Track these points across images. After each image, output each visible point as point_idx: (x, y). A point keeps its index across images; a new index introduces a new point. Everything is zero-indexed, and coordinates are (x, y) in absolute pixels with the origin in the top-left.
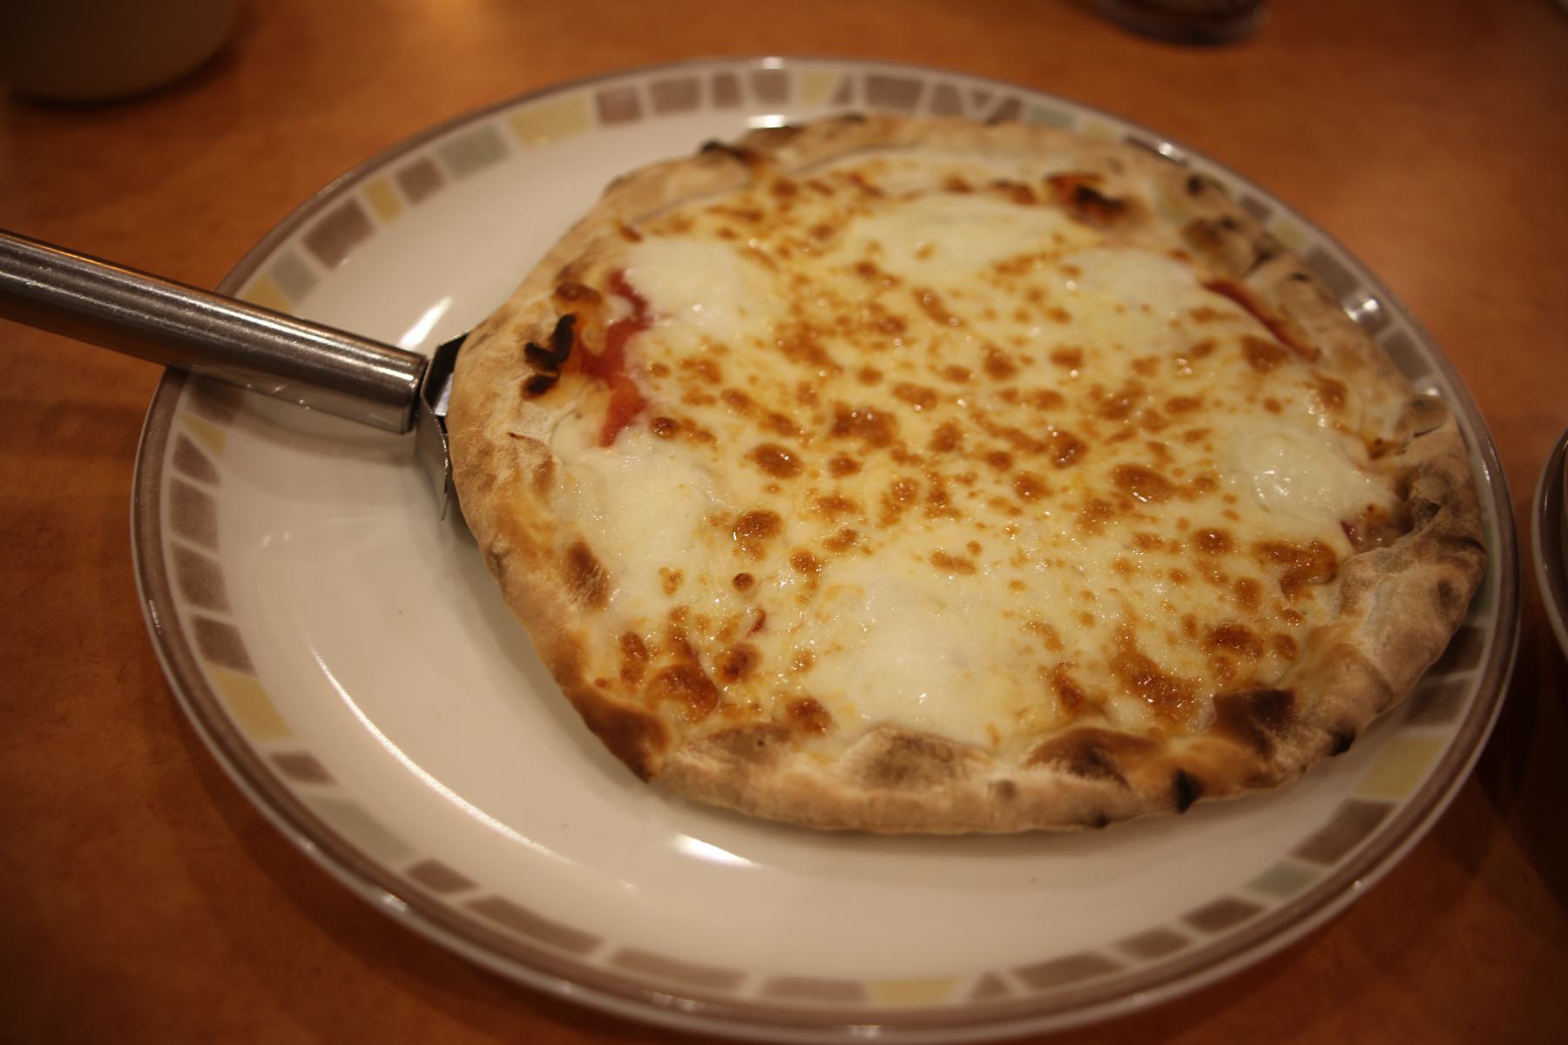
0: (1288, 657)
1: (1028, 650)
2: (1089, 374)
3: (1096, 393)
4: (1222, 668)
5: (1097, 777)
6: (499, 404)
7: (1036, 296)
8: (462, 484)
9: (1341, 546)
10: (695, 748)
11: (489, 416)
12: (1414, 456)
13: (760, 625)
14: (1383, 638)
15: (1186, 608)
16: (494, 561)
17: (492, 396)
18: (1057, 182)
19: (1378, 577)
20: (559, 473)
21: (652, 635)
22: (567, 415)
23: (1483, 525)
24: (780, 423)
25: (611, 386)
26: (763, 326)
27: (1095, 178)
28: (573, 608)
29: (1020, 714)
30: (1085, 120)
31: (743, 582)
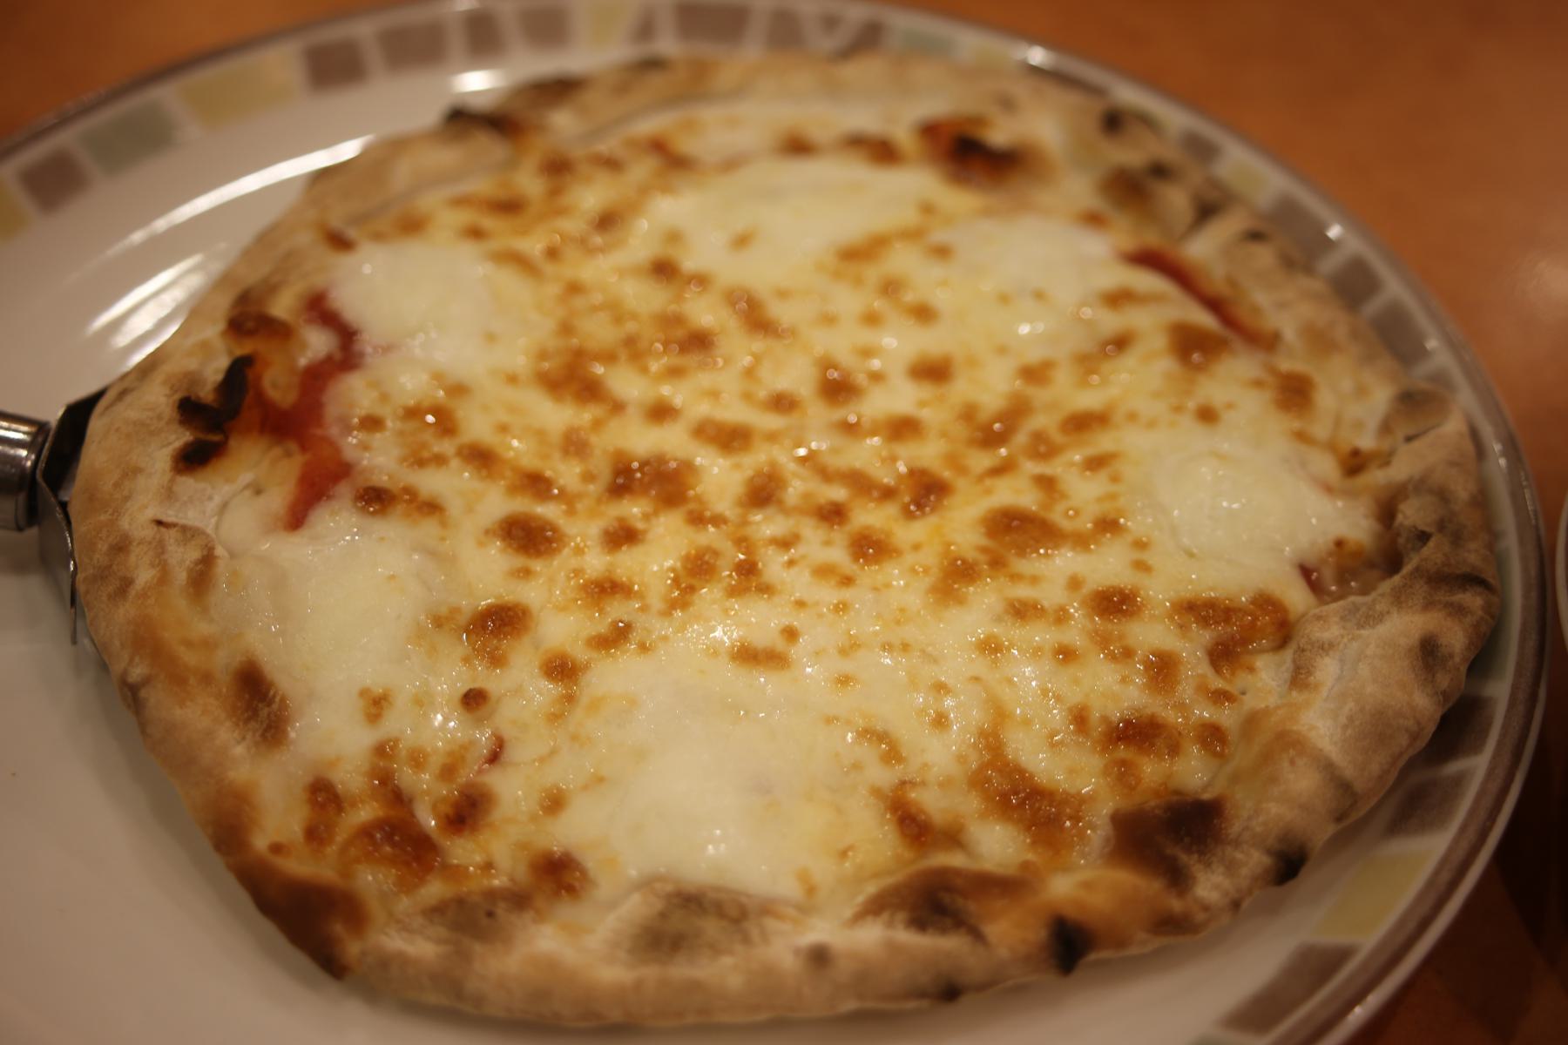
0: (1215, 754)
1: (857, 766)
2: (961, 389)
3: (968, 413)
4: (1123, 774)
5: (943, 931)
6: (141, 481)
7: (890, 288)
8: (87, 592)
9: (1296, 597)
10: (405, 928)
11: (127, 498)
12: (1401, 469)
13: (495, 757)
14: (1343, 720)
15: (1075, 696)
16: (129, 694)
17: (132, 472)
18: (930, 131)
19: (1342, 636)
20: (222, 568)
21: (351, 776)
22: (242, 491)
23: (1500, 562)
24: (536, 484)
25: (304, 448)
26: (519, 360)
27: (979, 121)
28: (239, 750)
29: (843, 854)
30: (971, 43)
31: (474, 700)
